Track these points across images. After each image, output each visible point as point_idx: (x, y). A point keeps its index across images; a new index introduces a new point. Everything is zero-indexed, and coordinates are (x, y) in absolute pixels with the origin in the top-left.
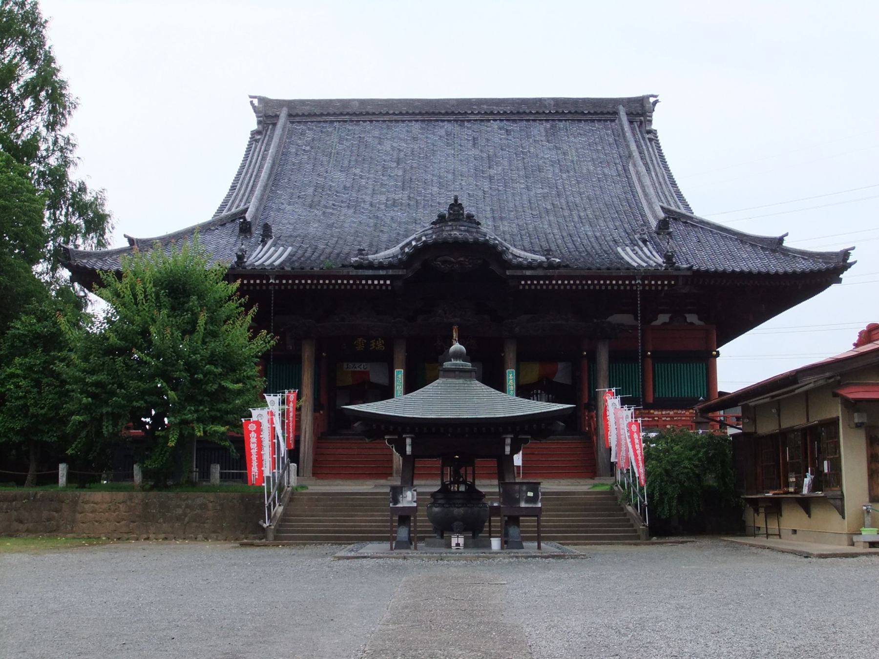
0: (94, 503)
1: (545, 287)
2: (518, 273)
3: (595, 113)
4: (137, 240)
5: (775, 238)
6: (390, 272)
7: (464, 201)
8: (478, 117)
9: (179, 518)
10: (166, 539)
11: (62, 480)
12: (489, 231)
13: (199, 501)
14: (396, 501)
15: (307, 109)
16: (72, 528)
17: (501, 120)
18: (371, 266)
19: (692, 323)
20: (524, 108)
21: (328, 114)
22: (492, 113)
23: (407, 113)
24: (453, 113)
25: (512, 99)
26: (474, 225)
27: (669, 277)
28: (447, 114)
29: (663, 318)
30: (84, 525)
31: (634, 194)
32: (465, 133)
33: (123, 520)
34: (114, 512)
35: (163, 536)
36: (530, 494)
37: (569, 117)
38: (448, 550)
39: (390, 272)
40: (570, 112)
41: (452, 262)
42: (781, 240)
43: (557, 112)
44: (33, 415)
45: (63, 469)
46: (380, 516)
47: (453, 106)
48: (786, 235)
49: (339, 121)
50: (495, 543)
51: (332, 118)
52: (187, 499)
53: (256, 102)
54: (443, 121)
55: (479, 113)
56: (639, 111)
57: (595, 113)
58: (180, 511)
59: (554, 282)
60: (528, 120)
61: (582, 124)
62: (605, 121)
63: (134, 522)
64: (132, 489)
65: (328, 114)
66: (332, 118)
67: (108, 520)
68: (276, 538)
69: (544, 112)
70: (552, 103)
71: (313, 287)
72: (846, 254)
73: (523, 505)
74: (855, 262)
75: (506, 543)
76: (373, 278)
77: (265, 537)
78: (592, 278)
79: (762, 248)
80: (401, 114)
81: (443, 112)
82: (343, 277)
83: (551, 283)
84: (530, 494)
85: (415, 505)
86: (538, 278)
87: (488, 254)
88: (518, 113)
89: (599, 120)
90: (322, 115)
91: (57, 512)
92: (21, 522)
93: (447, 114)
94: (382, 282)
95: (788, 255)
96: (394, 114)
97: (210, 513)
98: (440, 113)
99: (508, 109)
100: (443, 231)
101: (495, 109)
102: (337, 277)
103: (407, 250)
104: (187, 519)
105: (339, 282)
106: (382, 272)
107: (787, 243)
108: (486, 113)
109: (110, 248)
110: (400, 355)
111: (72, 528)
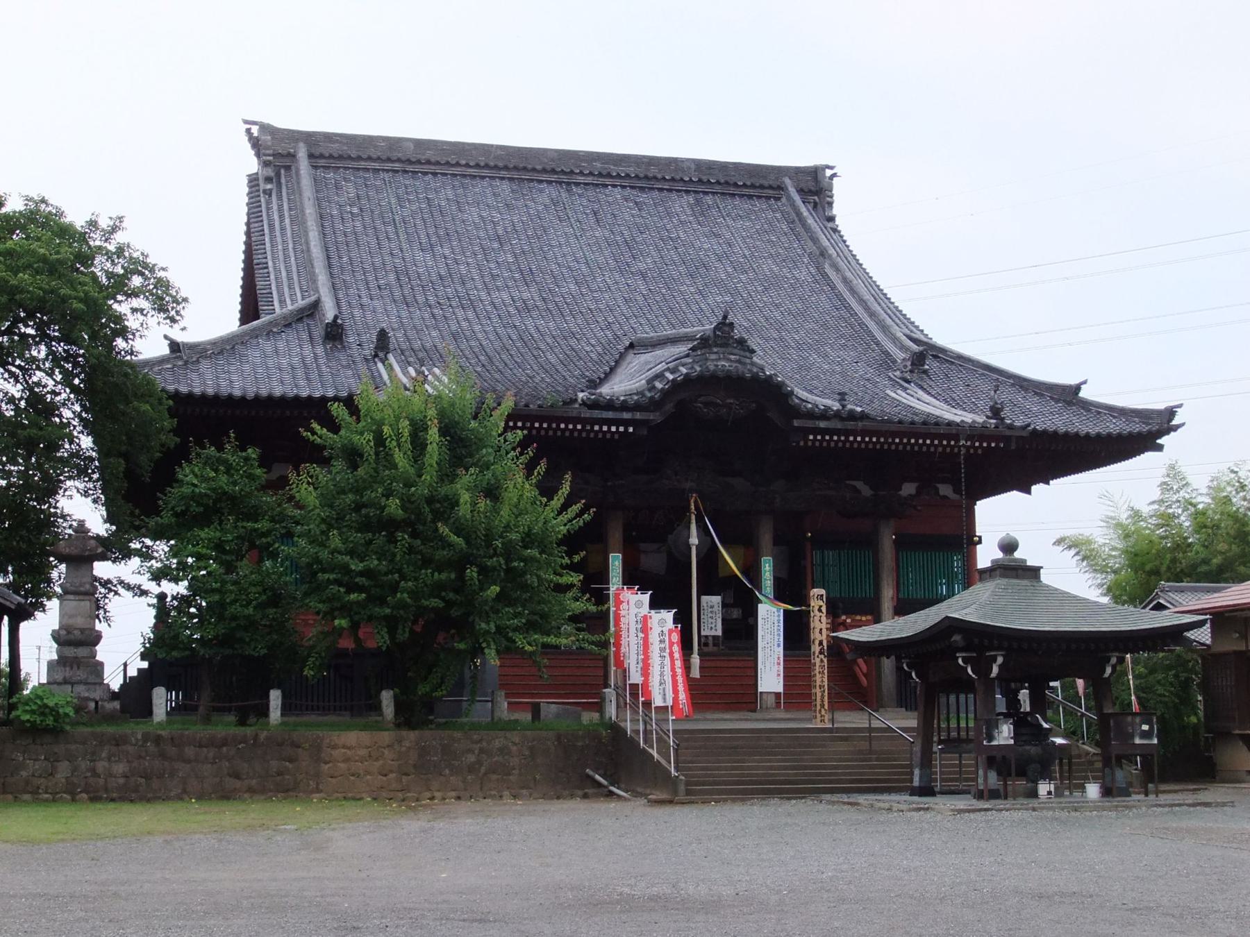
0: (344, 747)
1: (916, 448)
2: (810, 424)
3: (753, 186)
4: (184, 344)
5: (1070, 386)
6: (638, 416)
7: (736, 318)
8: (589, 180)
9: (471, 769)
10: (459, 798)
11: (275, 714)
12: (769, 360)
13: (497, 744)
14: (990, 738)
15: (334, 148)
16: (318, 784)
17: (623, 187)
18: (610, 405)
19: (945, 497)
20: (653, 171)
21: (370, 159)
22: (609, 175)
23: (487, 166)
24: (553, 171)
25: (636, 157)
26: (748, 354)
27: (998, 438)
28: (544, 171)
29: (908, 489)
30: (334, 780)
31: (848, 308)
32: (580, 202)
33: (391, 771)
34: (377, 759)
35: (454, 794)
36: (1145, 727)
37: (718, 189)
38: (1035, 801)
39: (638, 416)
40: (718, 183)
41: (717, 405)
42: (1078, 388)
43: (700, 180)
44: (234, 618)
45: (275, 697)
46: (778, 761)
47: (553, 160)
48: (1085, 382)
49: (388, 171)
50: (1093, 790)
51: (377, 165)
52: (480, 741)
53: (255, 130)
54: (541, 182)
55: (591, 174)
56: (814, 186)
57: (753, 186)
58: (471, 758)
59: (851, 438)
60: (661, 190)
61: (737, 201)
62: (768, 198)
63: (407, 774)
64: (378, 727)
65: (370, 159)
66: (377, 165)
67: (368, 773)
68: (688, 792)
69: (682, 179)
70: (693, 166)
71: (871, 446)
72: (1171, 413)
73: (1137, 741)
74: (1183, 424)
75: (1107, 792)
76: (610, 422)
77: (676, 793)
78: (901, 434)
79: (1052, 398)
80: (477, 166)
81: (539, 167)
82: (567, 420)
83: (847, 440)
84: (1145, 727)
85: (1012, 742)
86: (831, 432)
87: (770, 394)
88: (646, 177)
89: (759, 197)
90: (359, 158)
91: (291, 761)
92: (237, 776)
93: (544, 171)
94: (622, 429)
95: (1089, 410)
96: (467, 165)
97: (515, 761)
98: (534, 170)
99: (632, 171)
100: (707, 359)
101: (614, 170)
102: (559, 420)
103: (659, 385)
104: (483, 769)
105: (562, 426)
106: (626, 416)
107: (1084, 394)
108: (600, 175)
109: (141, 357)
110: (616, 535)
111: (318, 784)
